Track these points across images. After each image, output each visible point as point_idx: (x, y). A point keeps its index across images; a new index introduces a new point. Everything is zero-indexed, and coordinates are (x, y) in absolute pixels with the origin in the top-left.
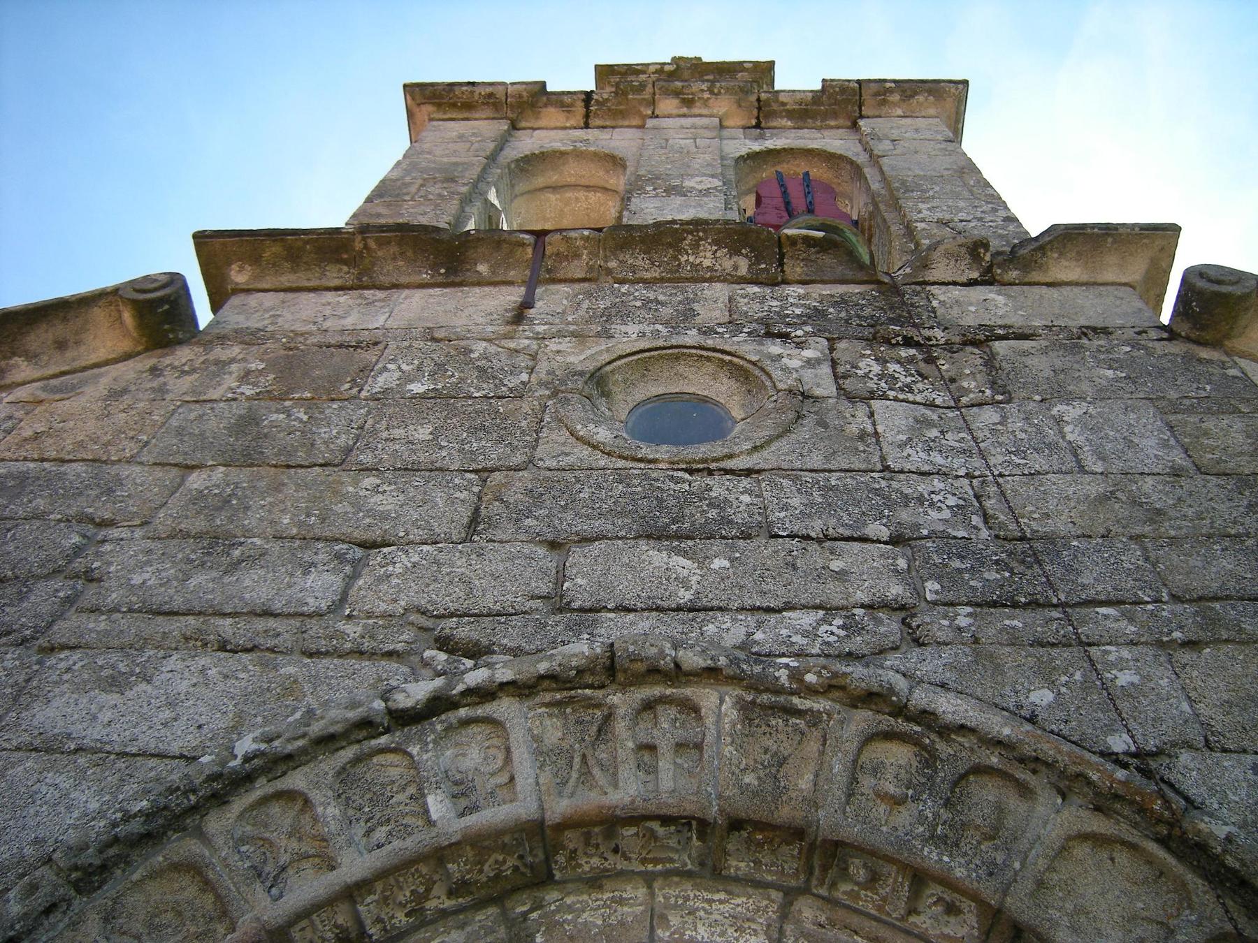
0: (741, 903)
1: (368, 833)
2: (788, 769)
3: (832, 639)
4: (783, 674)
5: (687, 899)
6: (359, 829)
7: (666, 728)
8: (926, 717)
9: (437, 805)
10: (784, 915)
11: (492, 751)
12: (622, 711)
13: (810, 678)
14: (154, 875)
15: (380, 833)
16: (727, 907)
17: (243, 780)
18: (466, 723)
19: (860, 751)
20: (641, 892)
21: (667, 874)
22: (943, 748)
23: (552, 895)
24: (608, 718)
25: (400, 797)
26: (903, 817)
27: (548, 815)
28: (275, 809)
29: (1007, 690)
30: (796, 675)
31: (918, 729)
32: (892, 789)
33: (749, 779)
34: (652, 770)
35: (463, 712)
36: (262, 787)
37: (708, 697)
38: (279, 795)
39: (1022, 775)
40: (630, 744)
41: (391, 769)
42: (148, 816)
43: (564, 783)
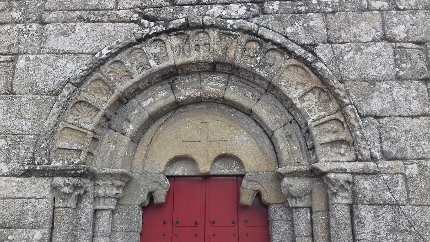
2: (229, 50)
5: (208, 76)
8: (261, 37)
9: (152, 63)
11: (162, 48)
12: (191, 37)
14: (93, 81)
15: (140, 69)
16: (216, 78)
19: (245, 45)
24: (188, 37)
27: (176, 64)
31: (259, 39)
32: (251, 55)
36: (111, 61)
37: (211, 32)
40: (193, 45)
42: (88, 70)
43: (179, 55)
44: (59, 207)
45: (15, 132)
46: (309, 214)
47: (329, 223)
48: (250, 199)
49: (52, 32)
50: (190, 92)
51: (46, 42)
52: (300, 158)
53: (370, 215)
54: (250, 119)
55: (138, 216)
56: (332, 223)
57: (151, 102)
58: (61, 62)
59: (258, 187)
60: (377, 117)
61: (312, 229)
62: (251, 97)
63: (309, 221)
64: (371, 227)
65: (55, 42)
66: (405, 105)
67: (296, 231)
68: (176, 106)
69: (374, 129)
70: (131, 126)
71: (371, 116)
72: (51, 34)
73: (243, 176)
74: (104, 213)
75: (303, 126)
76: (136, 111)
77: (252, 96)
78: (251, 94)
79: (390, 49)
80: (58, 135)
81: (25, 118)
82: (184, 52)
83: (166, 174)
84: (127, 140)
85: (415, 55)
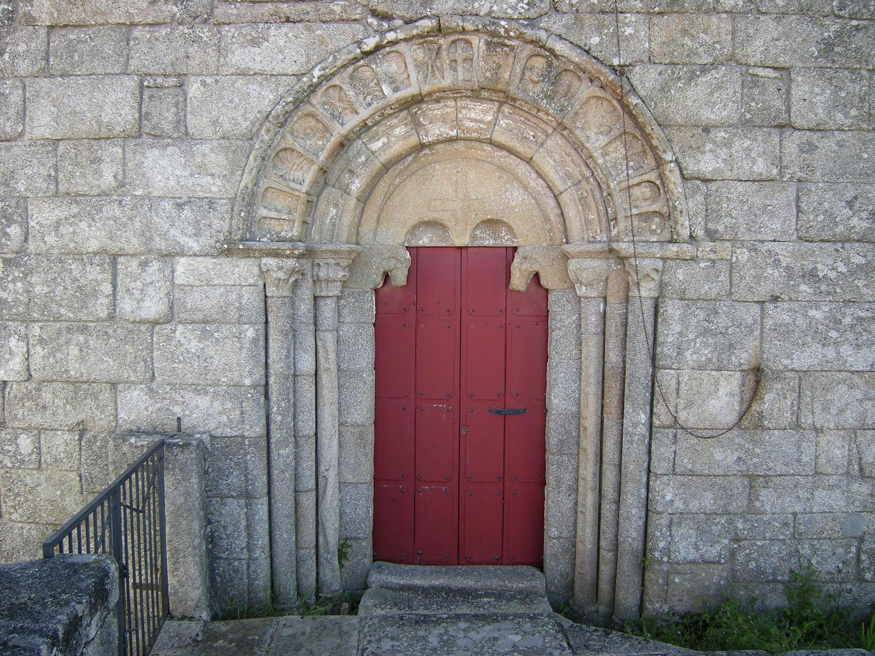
0: (485, 106)
1: (364, 99)
3: (523, 11)
4: (502, 31)
6: (361, 98)
7: (460, 53)
8: (551, 51)
9: (386, 89)
10: (499, 111)
12: (444, 47)
13: (512, 34)
15: (369, 99)
17: (319, 84)
18: (389, 53)
20: (453, 103)
21: (461, 97)
22: (555, 63)
23: (424, 106)
24: (439, 48)
25: (372, 84)
26: (538, 88)
28: (331, 91)
29: (583, 38)
30: (507, 31)
33: (488, 74)
34: (455, 70)
35: (388, 49)
37: (475, 39)
38: (331, 86)
39: (580, 74)
40: (448, 62)
41: (366, 73)
42: (294, 103)
44: (273, 297)
45: (201, 194)
46: (602, 306)
47: (627, 319)
48: (524, 282)
49: (234, 40)
50: (442, 129)
51: (226, 56)
52: (596, 231)
53: (678, 312)
54: (528, 167)
55: (370, 304)
56: (630, 320)
57: (384, 143)
58: (254, 88)
59: (536, 268)
60: (705, 181)
61: (605, 324)
62: (531, 138)
63: (602, 315)
64: (677, 328)
65: (240, 57)
66: (746, 165)
67: (583, 326)
68: (419, 147)
69: (700, 198)
70: (357, 181)
71: (698, 179)
72: (233, 43)
73: (515, 249)
74: (328, 301)
75: (604, 186)
76: (363, 158)
77: (534, 137)
78: (532, 133)
79: (736, 77)
80: (260, 198)
81: (212, 175)
82: (433, 72)
83: (406, 244)
84: (353, 202)
85: (772, 89)
